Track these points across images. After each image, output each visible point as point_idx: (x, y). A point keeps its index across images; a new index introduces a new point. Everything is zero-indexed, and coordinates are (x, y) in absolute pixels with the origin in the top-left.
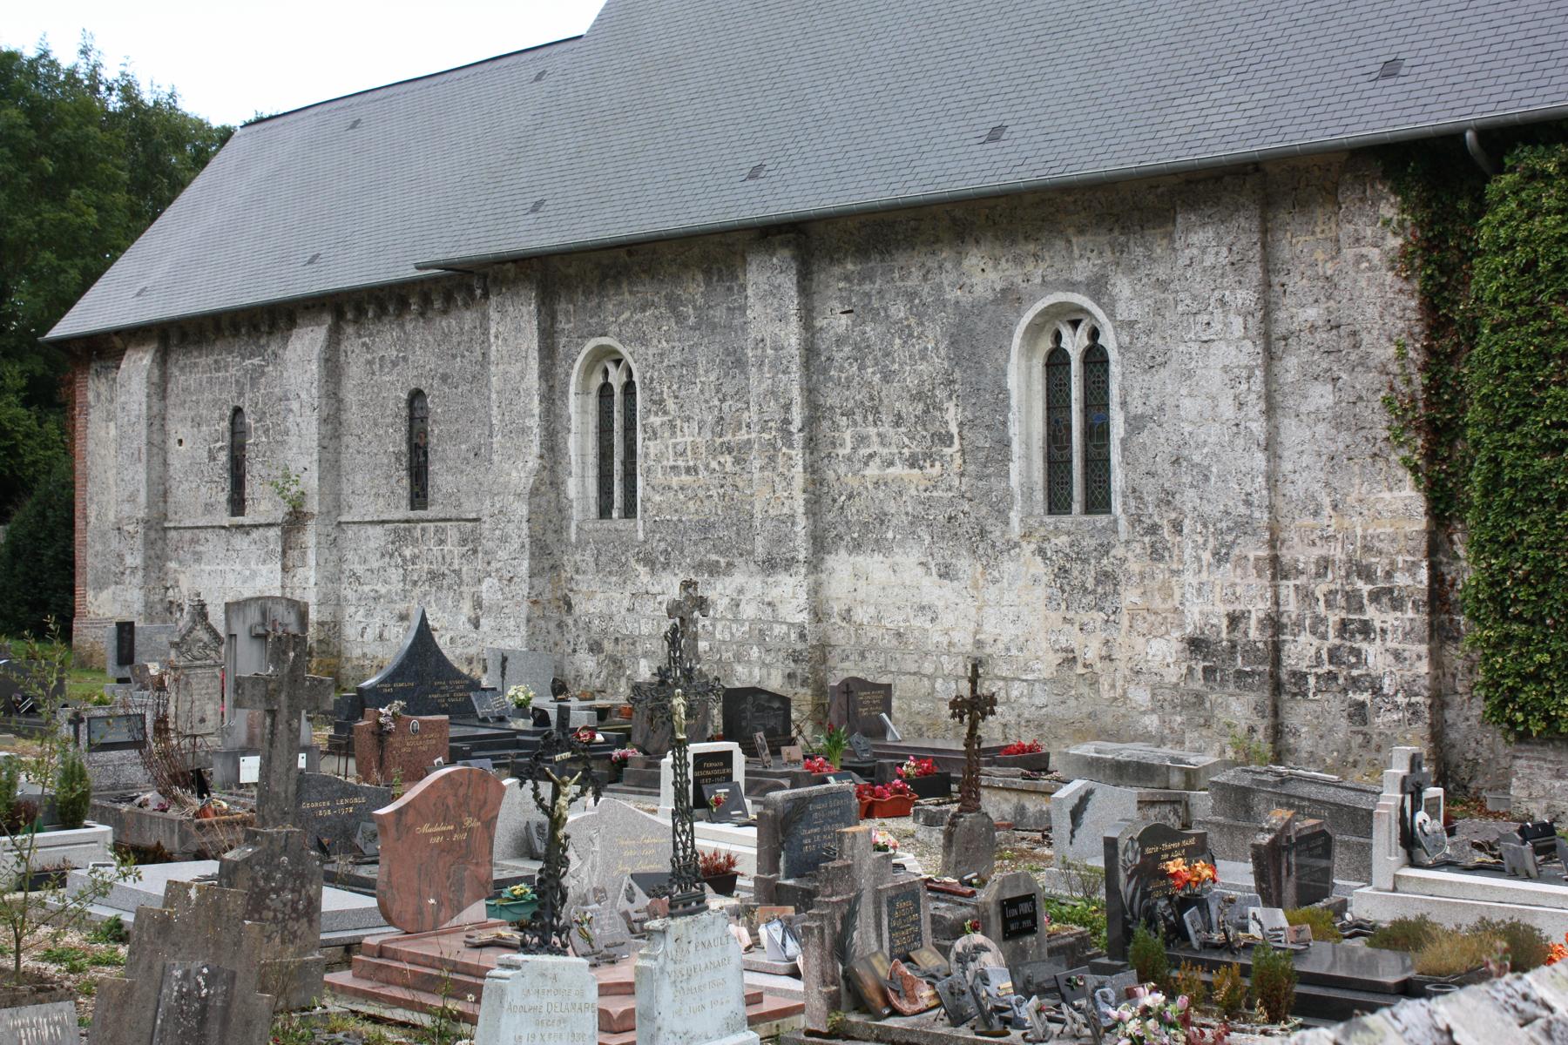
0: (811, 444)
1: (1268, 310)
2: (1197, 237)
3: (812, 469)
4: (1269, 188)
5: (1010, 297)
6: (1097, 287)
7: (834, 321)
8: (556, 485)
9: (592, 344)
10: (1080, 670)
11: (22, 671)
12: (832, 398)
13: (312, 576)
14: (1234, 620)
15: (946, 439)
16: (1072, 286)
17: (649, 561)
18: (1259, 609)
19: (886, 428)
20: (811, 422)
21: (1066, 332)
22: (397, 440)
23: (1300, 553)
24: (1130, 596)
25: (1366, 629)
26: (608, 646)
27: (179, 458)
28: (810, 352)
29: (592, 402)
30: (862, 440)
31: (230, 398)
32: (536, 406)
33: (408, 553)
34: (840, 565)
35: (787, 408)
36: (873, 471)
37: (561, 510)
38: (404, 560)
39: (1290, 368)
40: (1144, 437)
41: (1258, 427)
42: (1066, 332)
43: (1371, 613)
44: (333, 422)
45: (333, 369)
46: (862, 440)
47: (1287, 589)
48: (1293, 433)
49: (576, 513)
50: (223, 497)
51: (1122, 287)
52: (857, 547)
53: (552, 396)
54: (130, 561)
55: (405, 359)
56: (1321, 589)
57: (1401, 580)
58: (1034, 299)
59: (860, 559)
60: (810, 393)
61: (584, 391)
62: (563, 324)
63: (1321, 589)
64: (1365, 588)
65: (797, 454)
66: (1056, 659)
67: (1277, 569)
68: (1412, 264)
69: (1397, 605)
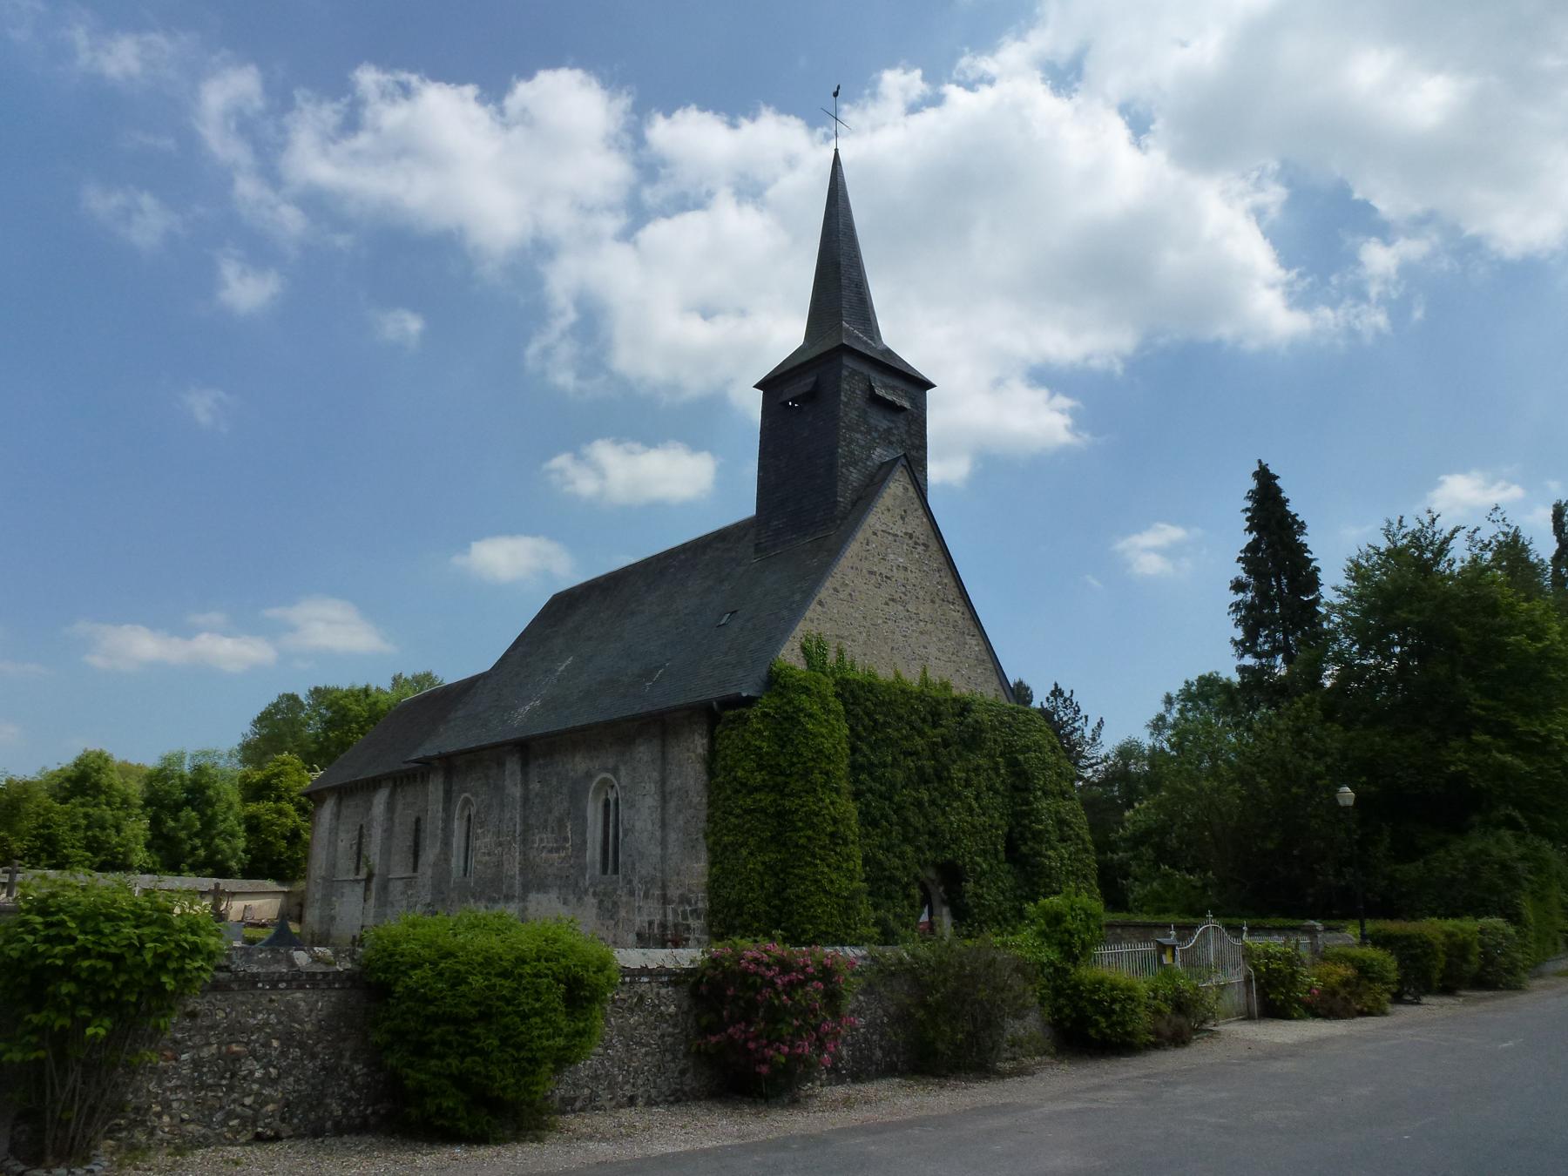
0: (524, 842)
1: (663, 782)
2: (642, 749)
3: (524, 854)
4: (660, 726)
5: (589, 776)
6: (615, 771)
7: (535, 786)
8: (447, 861)
10: (1343, 992)
12: (532, 821)
13: (850, 952)
14: (651, 923)
17: (474, 896)
18: (657, 919)
20: (524, 832)
22: (409, 843)
23: (674, 893)
25: (688, 928)
27: (341, 845)
28: (526, 800)
29: (464, 823)
32: (440, 824)
34: (533, 896)
37: (449, 872)
39: (672, 805)
41: (658, 834)
44: (389, 832)
45: (390, 807)
46: (541, 840)
47: (670, 908)
48: (672, 836)
49: (454, 874)
50: (353, 866)
51: (623, 771)
53: (448, 820)
57: (700, 905)
60: (525, 820)
61: (461, 817)
62: (455, 788)
64: (688, 908)
67: (665, 900)
68: (1123, 1009)
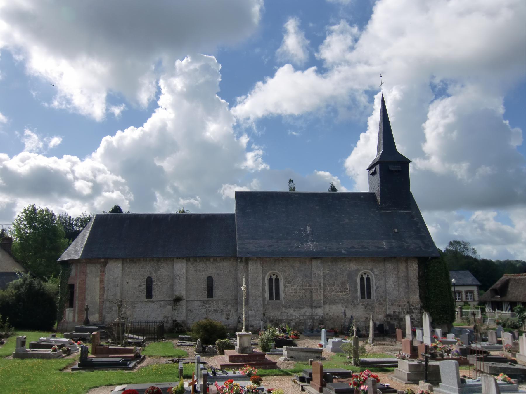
9: (271, 271)
11: (350, 351)
14: (394, 312)
15: (347, 289)
16: (368, 269)
19: (336, 287)
21: (272, 276)
24: (376, 310)
26: (274, 321)
30: (331, 289)
31: (148, 274)
33: (207, 306)
35: (320, 284)
36: (333, 293)
38: (206, 308)
40: (378, 289)
42: (272, 276)
43: (413, 311)
52: (330, 304)
54: (114, 308)
55: (207, 270)
56: (404, 308)
57: (417, 307)
58: (361, 270)
59: (331, 306)
63: (404, 308)
64: (412, 308)
65: (322, 291)
66: (365, 318)
69: (417, 309)
